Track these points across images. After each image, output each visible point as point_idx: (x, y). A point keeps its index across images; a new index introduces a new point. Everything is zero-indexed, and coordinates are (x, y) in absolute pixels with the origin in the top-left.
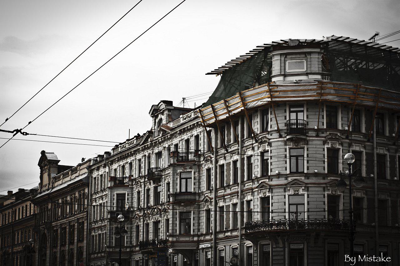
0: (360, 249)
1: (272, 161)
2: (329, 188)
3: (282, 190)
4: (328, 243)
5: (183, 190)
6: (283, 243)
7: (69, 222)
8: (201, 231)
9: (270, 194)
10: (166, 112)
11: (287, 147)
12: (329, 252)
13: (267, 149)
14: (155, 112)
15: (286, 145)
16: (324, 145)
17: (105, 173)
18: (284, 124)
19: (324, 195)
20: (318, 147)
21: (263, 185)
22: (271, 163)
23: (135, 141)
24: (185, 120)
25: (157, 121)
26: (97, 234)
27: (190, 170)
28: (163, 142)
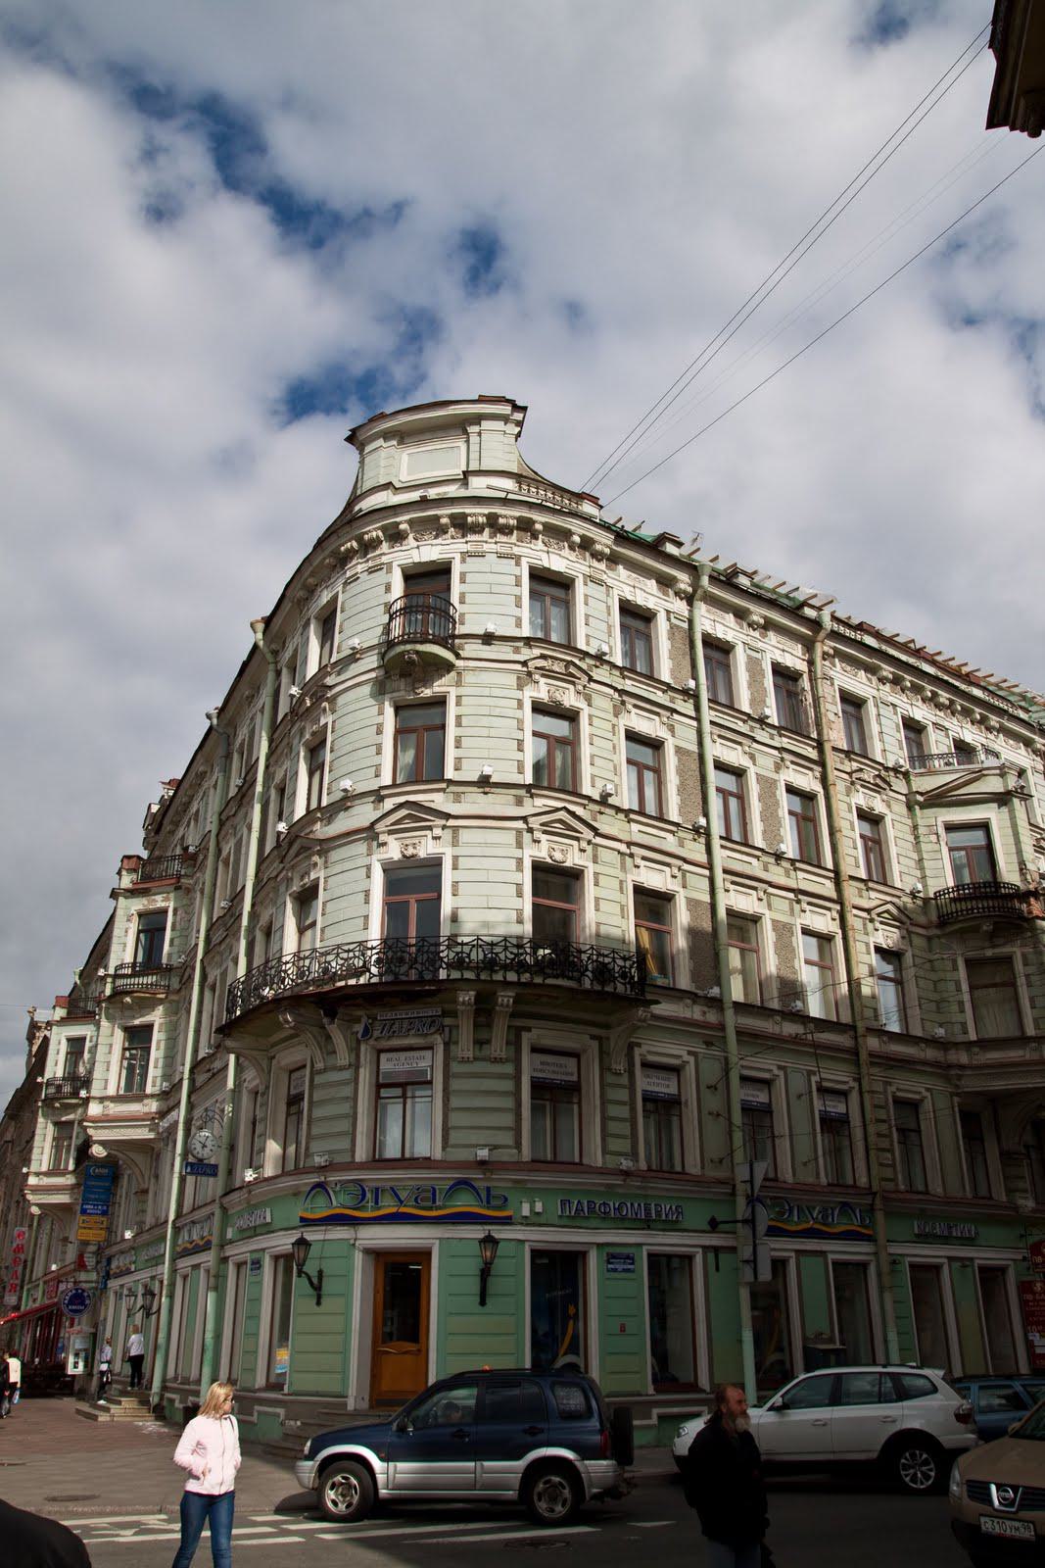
0: (668, 1086)
1: (466, 568)
2: (537, 835)
4: (535, 1050)
6: (350, 1050)
12: (538, 1086)
18: (460, 867)
19: (520, 861)
22: (463, 576)
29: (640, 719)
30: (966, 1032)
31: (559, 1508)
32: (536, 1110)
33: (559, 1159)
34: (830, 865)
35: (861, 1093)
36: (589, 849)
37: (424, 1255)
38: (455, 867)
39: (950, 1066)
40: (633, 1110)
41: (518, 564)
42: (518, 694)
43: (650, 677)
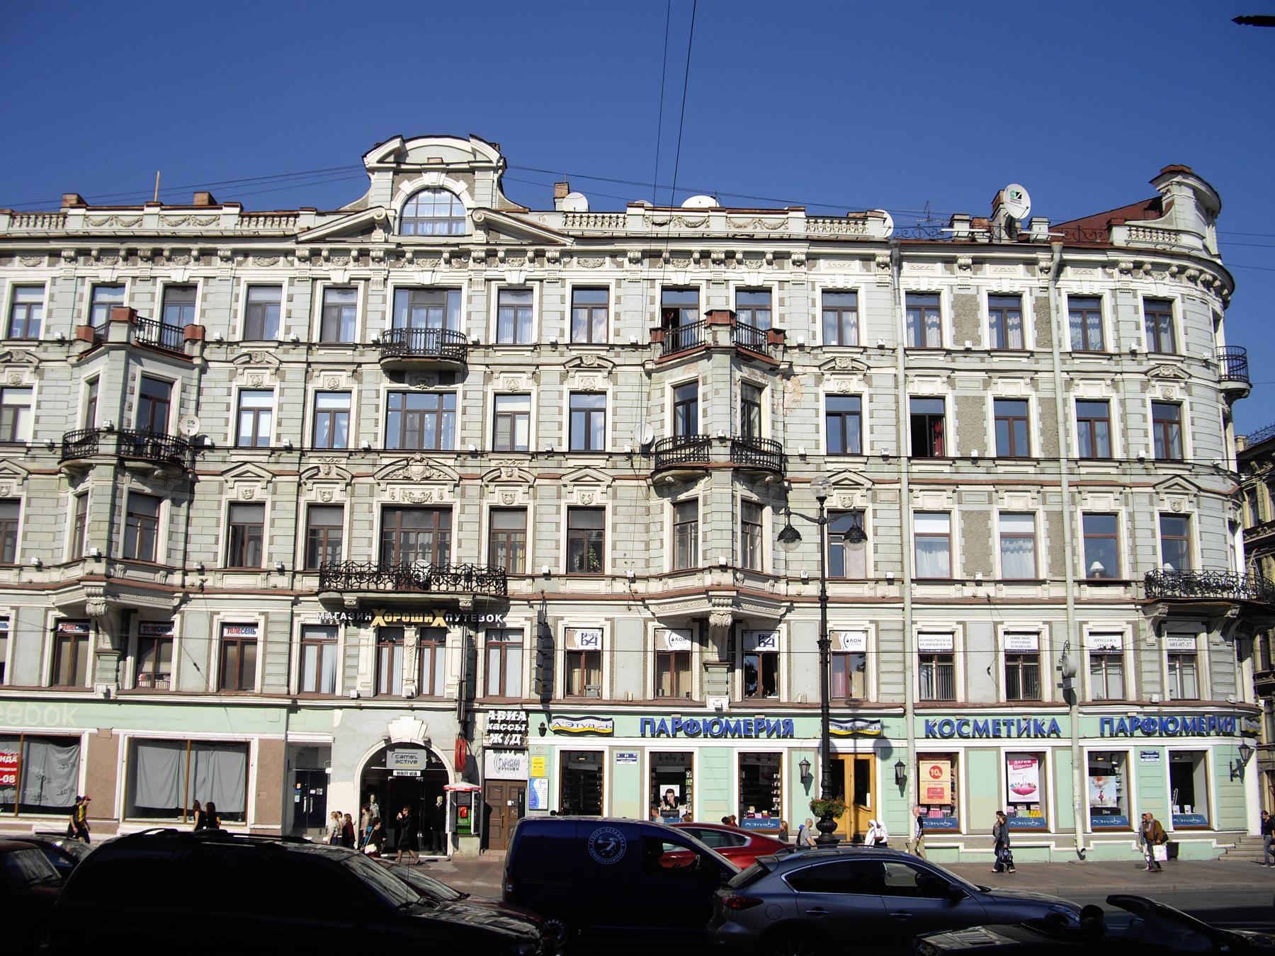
29: (923, 384)
32: (1172, 668)
33: (1186, 697)
36: (1194, 499)
37: (778, 756)
40: (1161, 665)
41: (1135, 296)
42: (1141, 396)
43: (1102, 353)
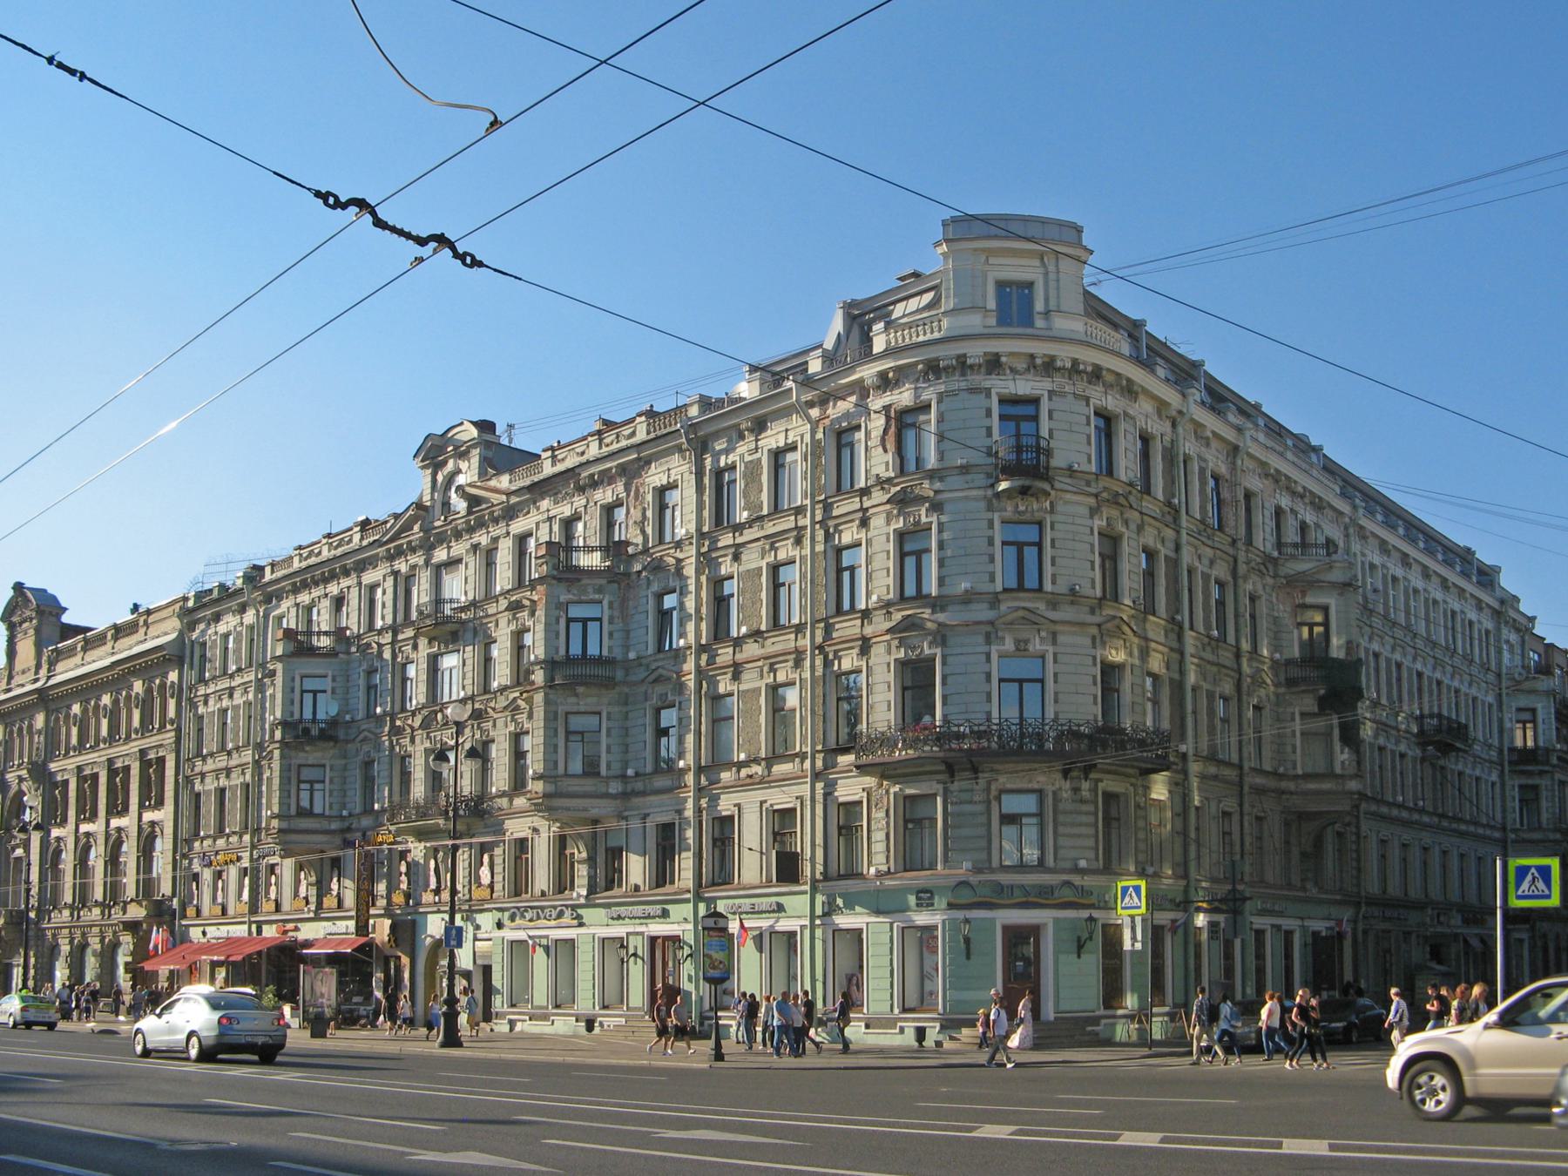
3: (981, 639)
5: (576, 650)
7: (109, 760)
8: (348, 806)
9: (938, 651)
10: (476, 452)
11: (996, 517)
13: (671, 584)
14: (434, 452)
15: (990, 508)
16: (1092, 517)
17: (239, 629)
20: (1078, 521)
21: (661, 676)
23: (357, 538)
24: (333, 552)
25: (440, 478)
26: (212, 787)
27: (597, 596)
28: (471, 530)
30: (1295, 768)
31: (1441, 1096)
34: (1233, 643)
35: (1242, 814)
38: (1055, 661)
39: (1283, 792)
42: (1089, 522)
